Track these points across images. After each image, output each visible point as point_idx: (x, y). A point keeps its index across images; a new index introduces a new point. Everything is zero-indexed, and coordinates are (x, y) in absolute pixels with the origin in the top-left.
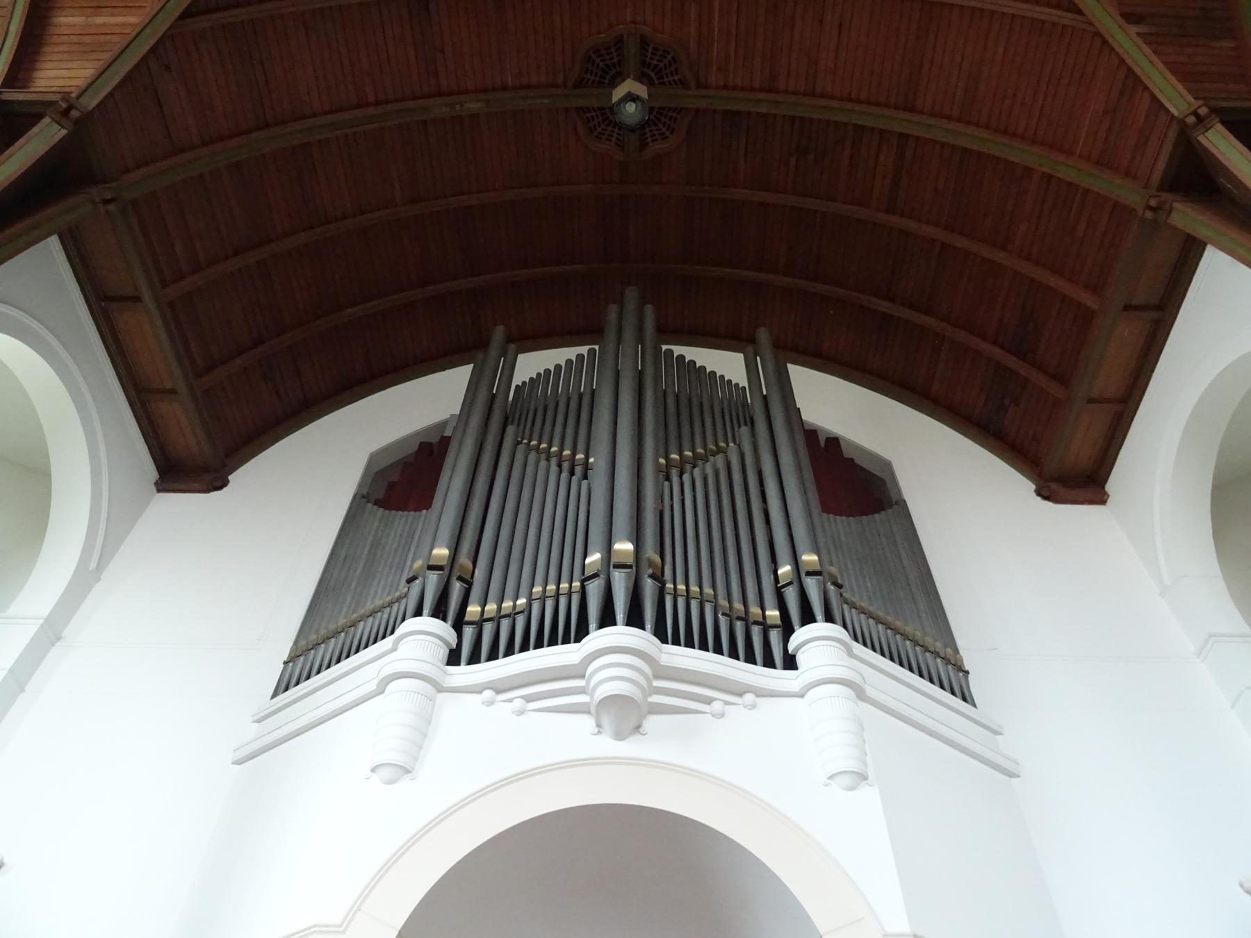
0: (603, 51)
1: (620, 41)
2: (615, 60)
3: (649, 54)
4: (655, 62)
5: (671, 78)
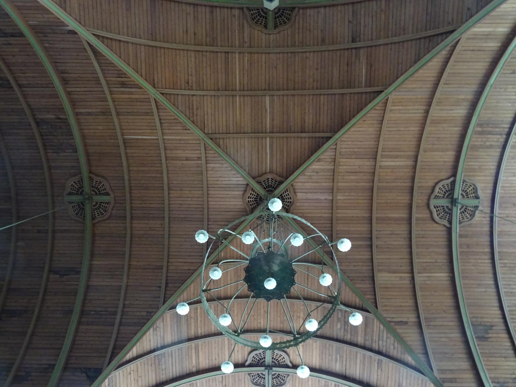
0: (282, 23)
1: (276, 27)
2: (277, 19)
3: (264, 22)
4: (261, 18)
5: (254, 12)
